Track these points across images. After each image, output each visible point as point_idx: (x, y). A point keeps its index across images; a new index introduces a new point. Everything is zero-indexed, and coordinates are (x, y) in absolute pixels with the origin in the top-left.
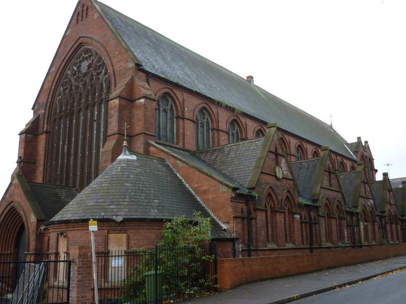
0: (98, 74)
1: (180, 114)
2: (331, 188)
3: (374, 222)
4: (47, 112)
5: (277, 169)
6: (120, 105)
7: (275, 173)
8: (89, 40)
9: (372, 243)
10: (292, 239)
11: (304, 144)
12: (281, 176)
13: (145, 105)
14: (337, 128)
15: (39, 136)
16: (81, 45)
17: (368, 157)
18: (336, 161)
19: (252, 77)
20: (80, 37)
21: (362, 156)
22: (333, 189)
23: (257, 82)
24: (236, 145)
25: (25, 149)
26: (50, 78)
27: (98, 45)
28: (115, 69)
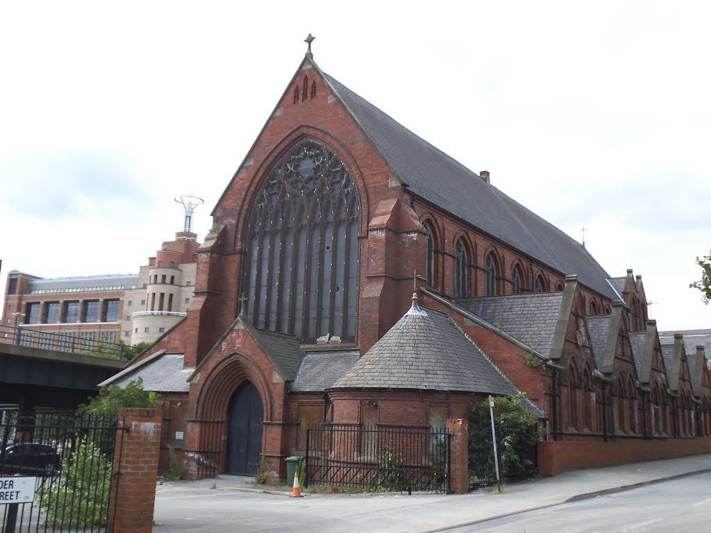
0: (333, 183)
3: (665, 405)
4: (240, 225)
6: (387, 239)
7: (576, 340)
9: (567, 430)
11: (472, 236)
14: (591, 249)
17: (641, 301)
18: (601, 308)
19: (488, 174)
20: (302, 125)
21: (633, 300)
22: (626, 359)
23: (495, 181)
26: (243, 174)
27: (335, 143)
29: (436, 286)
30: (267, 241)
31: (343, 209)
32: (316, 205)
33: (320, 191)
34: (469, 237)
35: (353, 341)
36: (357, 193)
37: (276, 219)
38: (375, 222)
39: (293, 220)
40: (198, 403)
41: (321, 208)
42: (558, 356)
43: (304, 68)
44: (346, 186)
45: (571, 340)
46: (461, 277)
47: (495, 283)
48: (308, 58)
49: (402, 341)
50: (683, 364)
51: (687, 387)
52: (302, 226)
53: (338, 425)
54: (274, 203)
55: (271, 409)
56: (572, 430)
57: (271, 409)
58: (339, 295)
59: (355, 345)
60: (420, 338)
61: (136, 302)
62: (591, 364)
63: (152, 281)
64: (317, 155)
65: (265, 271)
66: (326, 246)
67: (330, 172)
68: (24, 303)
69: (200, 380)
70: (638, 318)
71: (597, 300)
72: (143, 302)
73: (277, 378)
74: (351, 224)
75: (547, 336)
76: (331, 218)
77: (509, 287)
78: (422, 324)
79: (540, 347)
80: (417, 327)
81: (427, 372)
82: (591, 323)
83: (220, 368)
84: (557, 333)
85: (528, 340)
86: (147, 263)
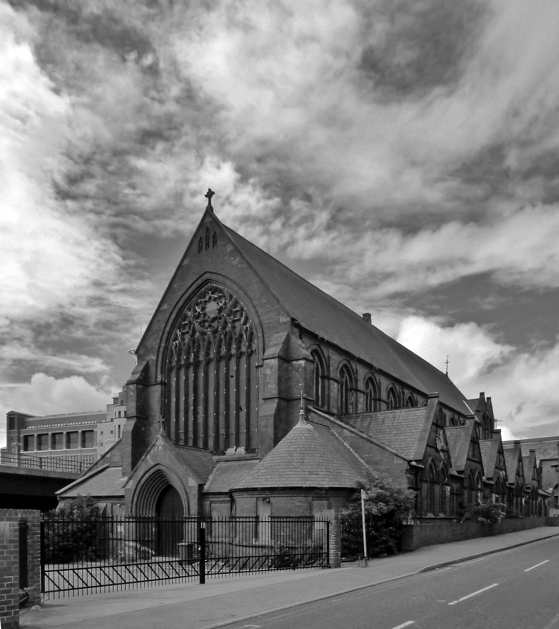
0: (234, 321)
1: (326, 374)
2: (473, 459)
5: (438, 442)
7: (436, 445)
8: (220, 279)
9: (426, 515)
10: (444, 509)
11: (354, 365)
12: (440, 448)
13: (305, 367)
15: (150, 388)
16: (207, 281)
20: (206, 272)
24: (391, 413)
25: (137, 403)
26: (162, 318)
27: (235, 287)
28: (261, 320)
29: (323, 405)
30: (182, 372)
31: (243, 343)
32: (221, 340)
33: (224, 328)
34: (351, 366)
35: (255, 452)
36: (254, 328)
37: (188, 354)
38: (269, 352)
39: (202, 354)
40: (132, 504)
41: (225, 344)
42: (421, 458)
43: (206, 221)
44: (245, 323)
45: (432, 445)
46: (344, 399)
47: (373, 403)
48: (209, 210)
49: (290, 449)
50: (519, 464)
51: (521, 481)
52: (210, 359)
53: (239, 518)
54: (186, 341)
55: (189, 506)
56: (430, 515)
57: (189, 506)
58: (243, 414)
59: (255, 455)
60: (305, 446)
61: (107, 432)
62: (448, 464)
63: (117, 416)
64: (220, 297)
65: (182, 398)
66: (230, 376)
67: (231, 311)
68: (22, 436)
69: (132, 486)
70: (487, 431)
71: (456, 417)
72: (112, 432)
73: (193, 483)
74: (250, 355)
75: (412, 442)
76: (233, 351)
77: (384, 406)
78: (308, 435)
79: (407, 451)
80: (303, 438)
81: (311, 473)
82: (449, 432)
83: (147, 475)
84: (420, 440)
85: (397, 446)
86: (111, 402)
